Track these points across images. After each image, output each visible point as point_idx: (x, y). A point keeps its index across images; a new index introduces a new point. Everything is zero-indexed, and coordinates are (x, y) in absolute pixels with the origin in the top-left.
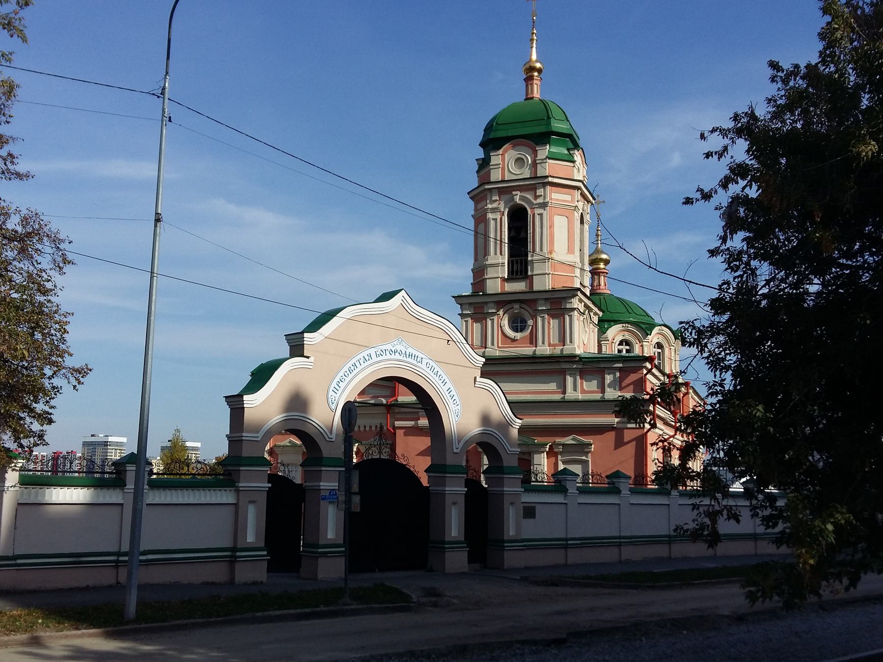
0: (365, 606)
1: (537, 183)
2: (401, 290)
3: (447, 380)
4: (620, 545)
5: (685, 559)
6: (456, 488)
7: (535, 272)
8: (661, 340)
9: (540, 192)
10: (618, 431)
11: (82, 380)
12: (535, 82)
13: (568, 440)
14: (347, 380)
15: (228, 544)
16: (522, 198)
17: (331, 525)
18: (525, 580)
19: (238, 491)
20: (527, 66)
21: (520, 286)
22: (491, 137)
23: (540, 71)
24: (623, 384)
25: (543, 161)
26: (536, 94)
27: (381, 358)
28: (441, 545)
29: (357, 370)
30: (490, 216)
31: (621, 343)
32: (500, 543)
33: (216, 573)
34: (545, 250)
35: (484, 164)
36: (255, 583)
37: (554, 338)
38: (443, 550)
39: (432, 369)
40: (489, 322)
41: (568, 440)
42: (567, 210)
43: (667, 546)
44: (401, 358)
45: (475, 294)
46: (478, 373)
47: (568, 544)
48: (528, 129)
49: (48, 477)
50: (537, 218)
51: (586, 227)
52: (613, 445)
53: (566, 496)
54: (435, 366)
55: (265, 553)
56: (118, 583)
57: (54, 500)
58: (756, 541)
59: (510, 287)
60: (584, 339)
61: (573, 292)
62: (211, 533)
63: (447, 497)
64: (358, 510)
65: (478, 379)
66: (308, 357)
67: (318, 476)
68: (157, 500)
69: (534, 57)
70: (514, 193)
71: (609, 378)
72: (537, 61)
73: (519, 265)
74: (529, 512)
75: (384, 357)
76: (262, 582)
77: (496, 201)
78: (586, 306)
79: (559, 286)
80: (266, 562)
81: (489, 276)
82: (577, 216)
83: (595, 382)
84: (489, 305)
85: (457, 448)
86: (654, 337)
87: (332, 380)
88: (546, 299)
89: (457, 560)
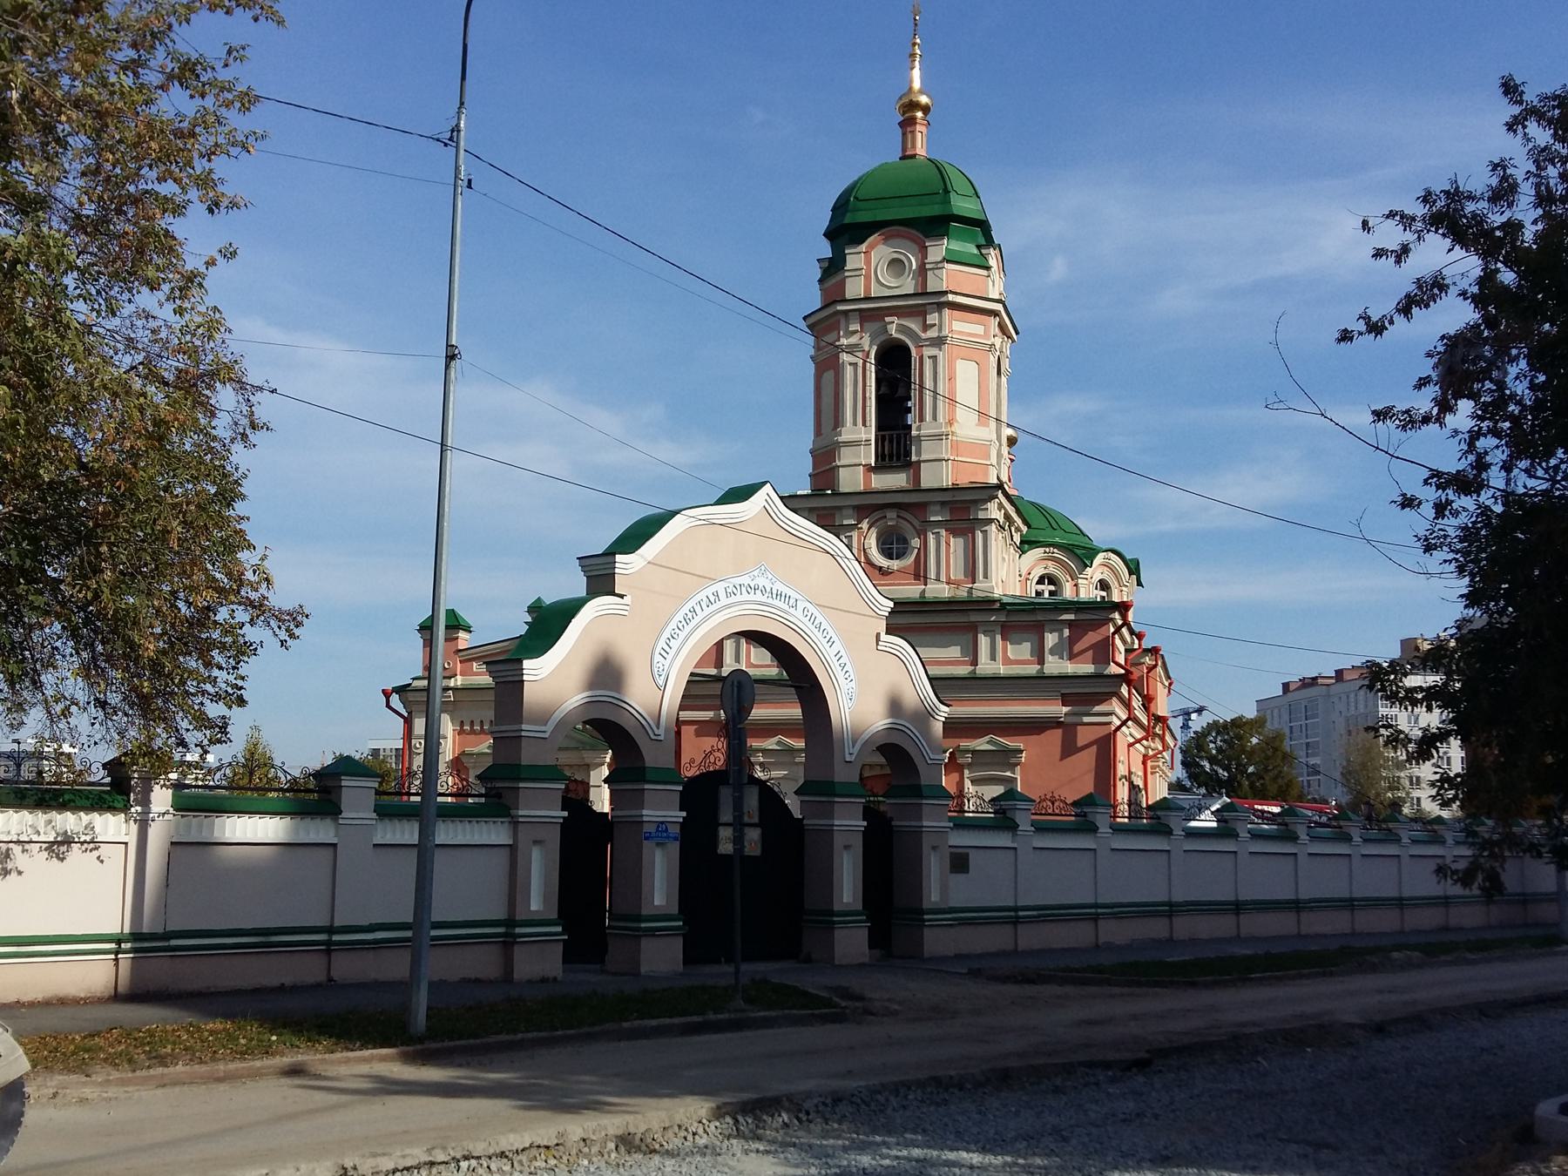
0: (780, 1013)
1: (928, 302)
2: (764, 483)
3: (835, 638)
4: (1095, 918)
5: (1194, 941)
6: (849, 822)
7: (923, 457)
8: (1107, 575)
9: (932, 318)
10: (1068, 729)
11: (297, 632)
12: (918, 128)
13: (982, 744)
14: (682, 635)
15: (500, 913)
16: (902, 329)
17: (660, 883)
18: (975, 974)
19: (515, 824)
20: (905, 100)
21: (896, 480)
22: (847, 221)
23: (926, 109)
24: (1077, 649)
25: (938, 266)
26: (921, 149)
27: (733, 599)
28: (827, 919)
29: (697, 619)
30: (845, 357)
31: (1040, 581)
32: (916, 915)
33: (480, 963)
34: (941, 418)
35: (833, 268)
36: (544, 980)
37: (957, 570)
38: (830, 927)
39: (812, 619)
40: (979, 535)
41: (982, 744)
42: (978, 350)
43: (1165, 921)
44: (764, 599)
45: (817, 492)
46: (882, 626)
47: (1018, 917)
48: (912, 210)
49: (223, 798)
50: (928, 364)
51: (1004, 379)
52: (1058, 756)
53: (1015, 835)
54: (816, 613)
55: (559, 929)
56: (330, 980)
57: (229, 836)
58: (1238, 914)
59: (881, 481)
60: (1010, 572)
61: (989, 491)
62: (466, 893)
63: (836, 835)
64: (758, 852)
65: (884, 637)
66: (622, 596)
67: (638, 800)
68: (389, 838)
69: (917, 85)
70: (887, 319)
71: (1051, 639)
72: (921, 92)
73: (896, 443)
74: (960, 863)
75: (739, 598)
76: (555, 979)
77: (855, 332)
78: (1007, 517)
79: (963, 481)
80: (560, 947)
81: (843, 462)
82: (993, 361)
83: (1027, 646)
84: (845, 512)
85: (851, 753)
86: (1096, 571)
87: (657, 638)
88: (943, 503)
89: (852, 942)
